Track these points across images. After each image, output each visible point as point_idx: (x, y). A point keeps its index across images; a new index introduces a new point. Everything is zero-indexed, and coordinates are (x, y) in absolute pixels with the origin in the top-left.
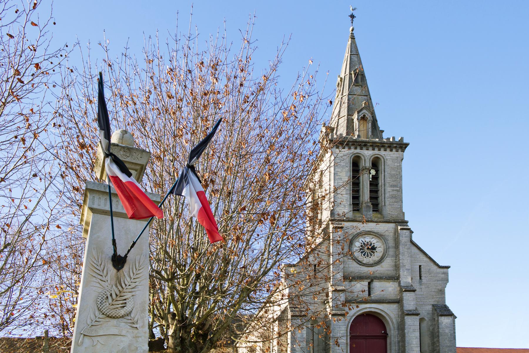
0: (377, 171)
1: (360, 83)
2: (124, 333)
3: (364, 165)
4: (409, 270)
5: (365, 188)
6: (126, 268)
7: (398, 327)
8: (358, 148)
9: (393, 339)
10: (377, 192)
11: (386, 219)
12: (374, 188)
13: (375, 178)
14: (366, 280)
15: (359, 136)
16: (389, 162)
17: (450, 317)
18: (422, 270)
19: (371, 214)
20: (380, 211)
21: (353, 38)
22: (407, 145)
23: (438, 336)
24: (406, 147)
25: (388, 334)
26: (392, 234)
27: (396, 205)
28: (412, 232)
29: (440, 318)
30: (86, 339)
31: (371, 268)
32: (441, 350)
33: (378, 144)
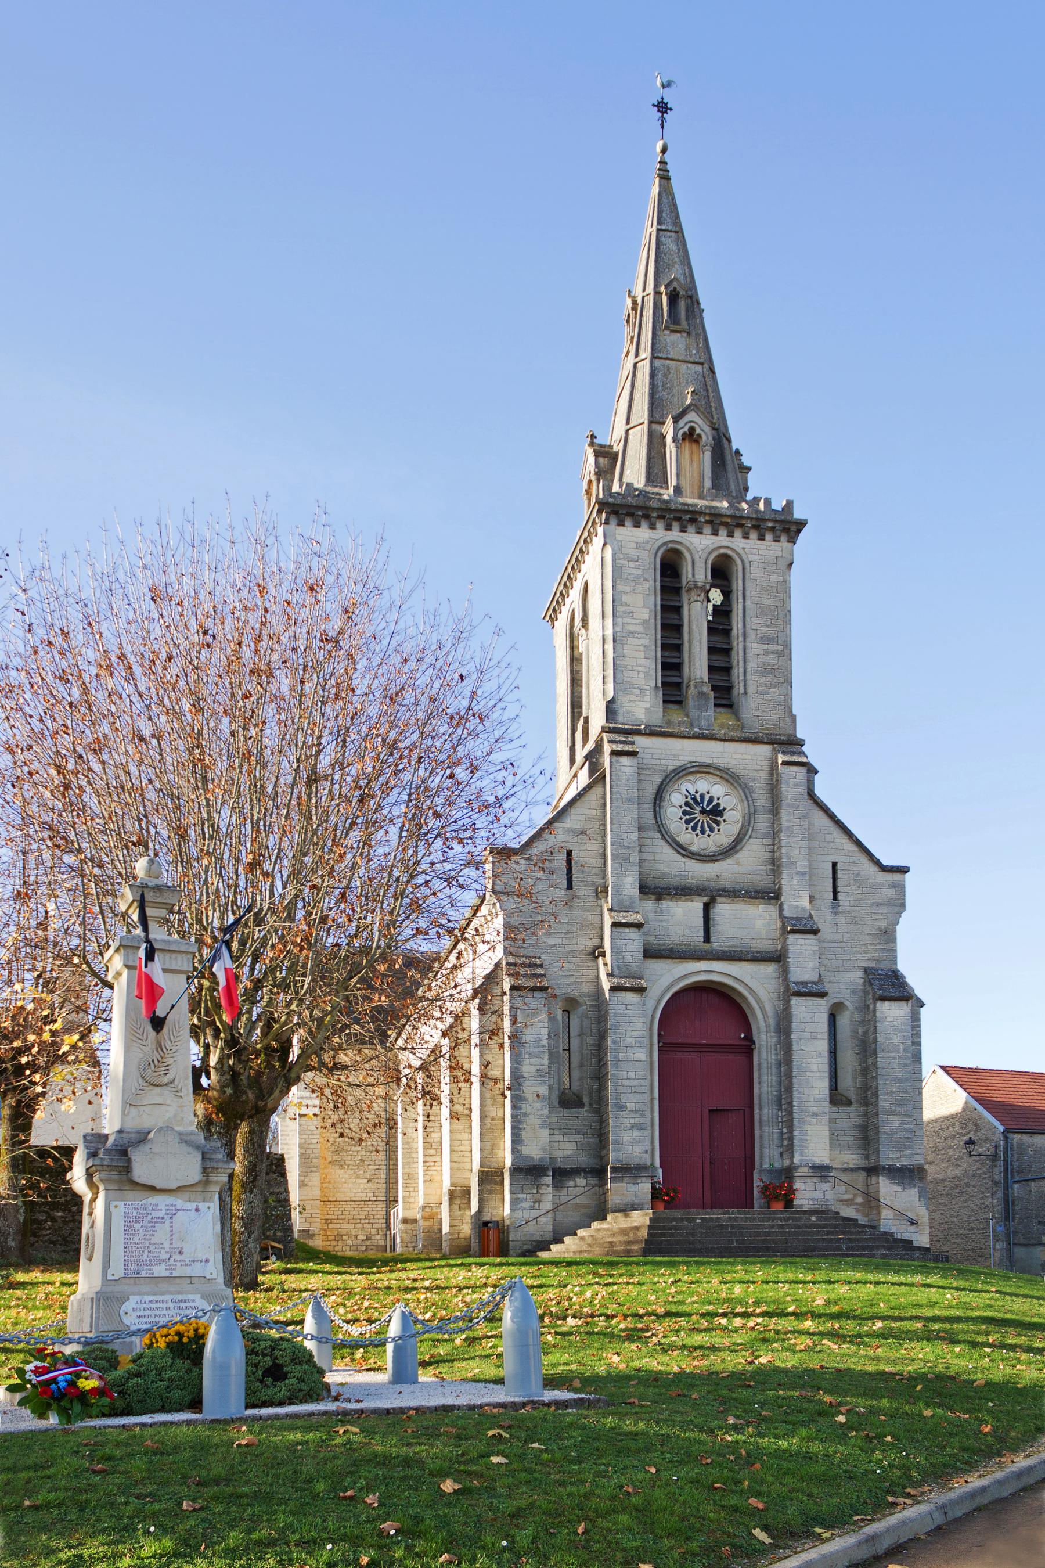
0: (727, 594)
1: (684, 324)
2: (168, 1102)
3: (690, 576)
4: (803, 874)
5: (696, 643)
6: (165, 1030)
7: (778, 1024)
8: (676, 525)
9: (764, 1055)
10: (727, 651)
11: (748, 732)
12: (719, 642)
13: (723, 612)
14: (697, 898)
15: (678, 490)
16: (755, 572)
17: (904, 1003)
18: (840, 874)
19: (709, 716)
20: (735, 706)
21: (664, 176)
22: (801, 525)
23: (875, 1053)
24: (799, 531)
25: (754, 1043)
26: (763, 775)
27: (774, 694)
28: (812, 771)
29: (879, 1004)
30: (132, 1108)
31: (711, 865)
32: (880, 1087)
33: (724, 520)
